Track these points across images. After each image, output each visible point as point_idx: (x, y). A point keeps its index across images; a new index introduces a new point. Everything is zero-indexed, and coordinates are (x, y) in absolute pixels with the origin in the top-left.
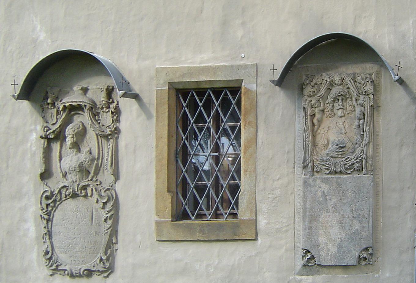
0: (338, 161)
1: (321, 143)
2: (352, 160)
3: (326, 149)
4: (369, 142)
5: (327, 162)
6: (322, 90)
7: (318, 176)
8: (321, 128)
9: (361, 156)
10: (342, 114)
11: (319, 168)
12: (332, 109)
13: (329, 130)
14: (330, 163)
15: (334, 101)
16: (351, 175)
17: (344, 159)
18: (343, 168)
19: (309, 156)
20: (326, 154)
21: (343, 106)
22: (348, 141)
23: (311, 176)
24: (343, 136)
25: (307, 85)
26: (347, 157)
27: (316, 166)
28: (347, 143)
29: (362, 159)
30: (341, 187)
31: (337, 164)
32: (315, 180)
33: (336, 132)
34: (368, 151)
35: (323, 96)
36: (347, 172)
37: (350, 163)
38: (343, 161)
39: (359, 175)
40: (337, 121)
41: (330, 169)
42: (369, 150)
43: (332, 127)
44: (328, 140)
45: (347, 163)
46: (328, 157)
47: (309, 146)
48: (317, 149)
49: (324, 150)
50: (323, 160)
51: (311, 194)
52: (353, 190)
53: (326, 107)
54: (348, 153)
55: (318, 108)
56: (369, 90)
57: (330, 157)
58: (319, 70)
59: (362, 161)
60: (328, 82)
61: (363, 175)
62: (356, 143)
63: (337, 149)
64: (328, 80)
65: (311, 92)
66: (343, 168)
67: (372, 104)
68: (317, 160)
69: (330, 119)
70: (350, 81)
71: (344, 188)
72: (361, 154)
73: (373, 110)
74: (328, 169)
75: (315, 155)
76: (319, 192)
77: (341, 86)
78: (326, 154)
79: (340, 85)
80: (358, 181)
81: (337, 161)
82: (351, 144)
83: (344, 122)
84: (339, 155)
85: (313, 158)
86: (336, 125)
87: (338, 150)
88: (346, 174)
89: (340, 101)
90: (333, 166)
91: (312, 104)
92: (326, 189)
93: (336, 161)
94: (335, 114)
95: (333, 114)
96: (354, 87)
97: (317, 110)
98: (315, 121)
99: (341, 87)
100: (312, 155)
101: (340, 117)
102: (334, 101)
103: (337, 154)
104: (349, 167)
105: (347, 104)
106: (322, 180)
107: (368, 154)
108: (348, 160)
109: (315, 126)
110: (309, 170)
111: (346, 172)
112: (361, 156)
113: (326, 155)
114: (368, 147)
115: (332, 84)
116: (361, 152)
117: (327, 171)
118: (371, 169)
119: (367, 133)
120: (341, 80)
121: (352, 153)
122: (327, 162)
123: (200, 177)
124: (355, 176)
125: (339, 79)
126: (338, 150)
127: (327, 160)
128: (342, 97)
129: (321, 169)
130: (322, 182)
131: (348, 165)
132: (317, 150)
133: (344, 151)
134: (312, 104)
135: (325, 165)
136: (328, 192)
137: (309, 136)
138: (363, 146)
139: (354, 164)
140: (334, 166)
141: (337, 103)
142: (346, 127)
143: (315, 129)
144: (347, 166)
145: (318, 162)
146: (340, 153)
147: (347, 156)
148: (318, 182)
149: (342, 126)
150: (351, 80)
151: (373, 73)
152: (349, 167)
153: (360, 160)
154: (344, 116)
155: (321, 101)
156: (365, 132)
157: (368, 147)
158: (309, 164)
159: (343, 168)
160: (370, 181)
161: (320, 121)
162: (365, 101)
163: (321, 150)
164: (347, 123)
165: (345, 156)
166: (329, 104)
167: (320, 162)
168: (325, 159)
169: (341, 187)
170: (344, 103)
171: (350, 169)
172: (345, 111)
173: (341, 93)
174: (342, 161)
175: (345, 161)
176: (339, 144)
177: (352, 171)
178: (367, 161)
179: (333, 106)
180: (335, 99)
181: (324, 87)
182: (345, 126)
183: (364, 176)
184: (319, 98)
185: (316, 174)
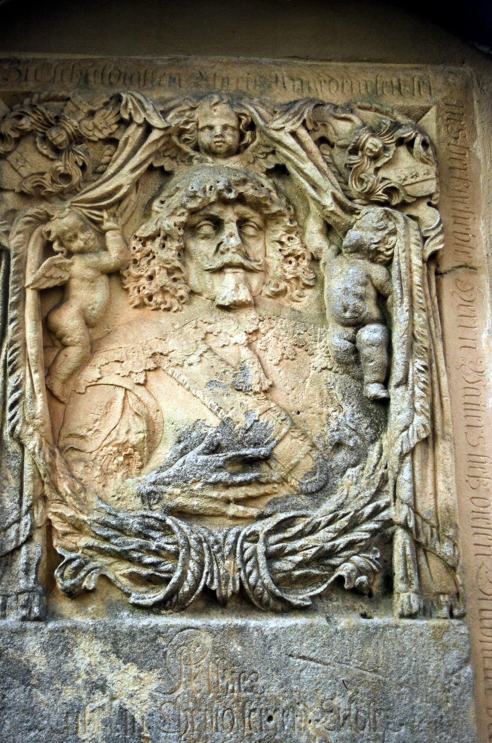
0: (225, 537)
1: (103, 435)
2: (322, 534)
3: (134, 470)
4: (429, 441)
5: (147, 537)
6: (122, 167)
7: (83, 620)
8: (100, 360)
9: (377, 511)
10: (243, 295)
11: (94, 576)
12: (178, 264)
13: (160, 373)
14: (176, 543)
15: (190, 229)
16: (319, 620)
17: (262, 527)
18: (259, 577)
19: (26, 504)
20: (141, 495)
21: (246, 256)
22: (284, 430)
23: (37, 619)
24: (250, 401)
25: (18, 141)
26: (282, 516)
27: (74, 564)
28: (278, 442)
29: (390, 530)
30: (251, 689)
31: (220, 550)
32: (62, 644)
33: (205, 379)
34: (424, 486)
35: (120, 201)
36: (285, 596)
37: (303, 548)
38: (262, 536)
39: (364, 616)
40: (209, 328)
41: (174, 580)
42: (430, 481)
43: (177, 356)
44: (149, 421)
45: (290, 546)
46: (157, 515)
47: (22, 446)
48: (79, 469)
49: (119, 475)
50: (121, 529)
51: (30, 730)
52: (335, 702)
53: (138, 256)
54: (283, 491)
55: (92, 259)
56: (410, 181)
57: (172, 511)
58: (91, 78)
59: (383, 538)
60: (155, 135)
61: (402, 616)
62: (338, 445)
63: (219, 468)
64: (156, 121)
65: (47, 176)
66: (264, 572)
67: (441, 246)
68: (78, 527)
69: (165, 319)
70: (294, 134)
71: (274, 690)
72: (382, 502)
73: (438, 282)
74: (152, 581)
75: (63, 501)
76: (88, 716)
77: (235, 158)
78: (141, 495)
79: (230, 153)
80: (369, 651)
81: (220, 536)
82: (306, 447)
83: (256, 331)
84: (228, 502)
85: (52, 517)
86: (203, 347)
87: (223, 476)
88: (277, 612)
89: (231, 228)
90: (191, 564)
91: (49, 233)
92: (145, 695)
93: (211, 533)
94: (192, 293)
95: (182, 292)
96: (319, 168)
97: (79, 266)
98: (68, 319)
99: (234, 162)
100: (44, 498)
101: (223, 308)
102: (190, 229)
103: (214, 494)
104: (297, 573)
105: (268, 249)
106: (114, 643)
107: (426, 504)
108: (294, 530)
109: (65, 346)
110: (22, 584)
111: (280, 599)
112: (377, 511)
113: (139, 500)
114: (424, 463)
115: (179, 146)
116: (379, 492)
117: (143, 589)
118: (452, 588)
119: (418, 392)
120: (233, 128)
121: (310, 494)
122: (147, 537)
123: (314, 576)
124: (343, 622)
125: (225, 122)
126: (223, 476)
127: (152, 528)
128: (241, 209)
129: (103, 577)
130: (117, 653)
131: (298, 558)
132: (78, 475)
133: (262, 484)
134: (53, 236)
135: (135, 555)
136: (156, 718)
137: (28, 394)
138: (394, 459)
139: (332, 553)
140: (201, 565)
141: (206, 237)
142: (271, 357)
143: (64, 368)
144: (290, 566)
145: (84, 541)
146: (241, 492)
147: (285, 509)
148: (87, 655)
149: (245, 353)
150: (302, 132)
151: (428, 109)
152: (297, 573)
153: (374, 532)
154: (253, 304)
155: (107, 225)
156: (404, 382)
157: (424, 463)
158: (18, 548)
159: (259, 577)
160: (455, 653)
161: (98, 328)
162: (393, 233)
163: (105, 474)
164: (273, 341)
165: (268, 511)
166: (158, 240)
167: (97, 536)
168: (134, 524)
169: (251, 689)
170: (251, 241)
171: (307, 580)
172: (255, 280)
173: (241, 189)
174: (253, 537)
175: (273, 539)
176: (224, 443)
177: (319, 591)
178: (422, 540)
179: (183, 252)
180: (196, 219)
181: (134, 152)
182: (262, 354)
183: (404, 628)
184: (100, 209)
185: (66, 606)
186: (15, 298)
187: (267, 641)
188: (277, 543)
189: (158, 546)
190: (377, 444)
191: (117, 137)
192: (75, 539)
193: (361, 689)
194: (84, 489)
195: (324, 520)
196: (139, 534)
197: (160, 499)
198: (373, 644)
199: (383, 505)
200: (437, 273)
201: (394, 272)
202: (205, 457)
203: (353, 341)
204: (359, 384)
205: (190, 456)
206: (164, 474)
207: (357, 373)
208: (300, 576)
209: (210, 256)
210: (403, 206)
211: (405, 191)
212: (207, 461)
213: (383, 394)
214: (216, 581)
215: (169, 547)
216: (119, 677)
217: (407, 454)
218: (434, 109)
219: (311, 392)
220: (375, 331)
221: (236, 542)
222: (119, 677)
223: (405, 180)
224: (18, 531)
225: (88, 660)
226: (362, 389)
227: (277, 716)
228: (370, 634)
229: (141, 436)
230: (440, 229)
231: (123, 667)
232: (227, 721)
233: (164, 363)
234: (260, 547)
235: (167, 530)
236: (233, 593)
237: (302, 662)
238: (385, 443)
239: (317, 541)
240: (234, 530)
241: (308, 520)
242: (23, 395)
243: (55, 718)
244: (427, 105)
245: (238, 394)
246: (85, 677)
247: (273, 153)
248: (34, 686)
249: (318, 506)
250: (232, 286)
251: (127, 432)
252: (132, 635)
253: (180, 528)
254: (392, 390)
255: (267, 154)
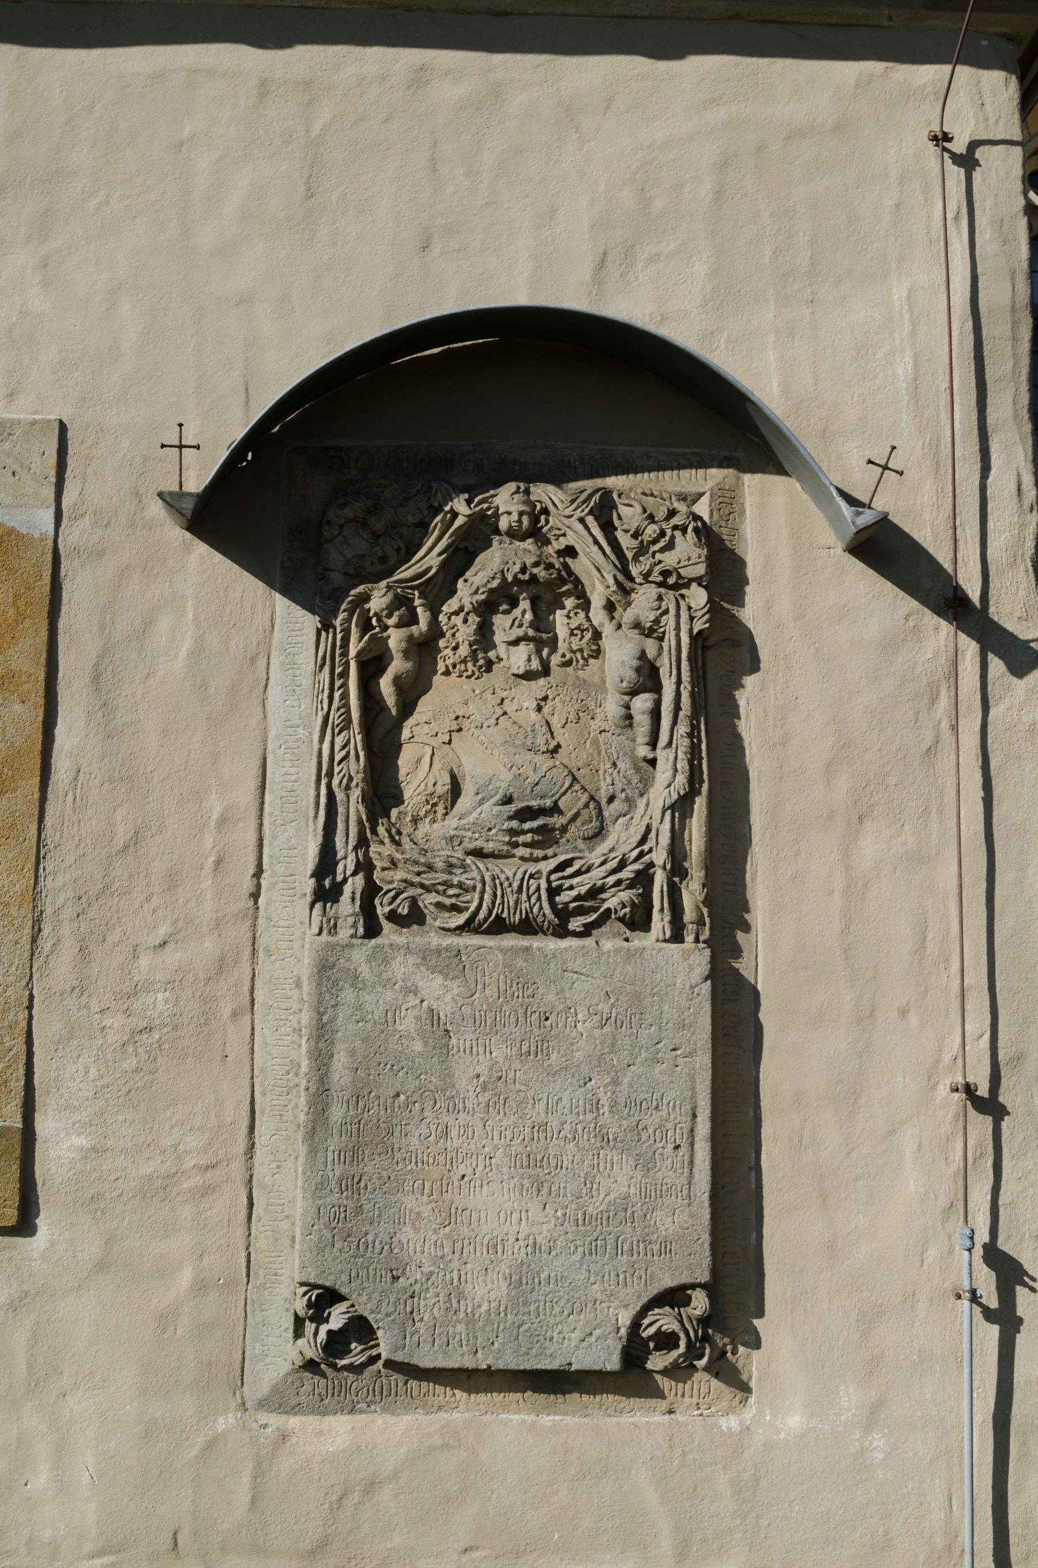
5: (450, 873)
16: (589, 942)
22: (567, 785)
26: (562, 858)
37: (579, 885)
40: (504, 694)
44: (454, 778)
45: (567, 883)
46: (459, 855)
49: (428, 820)
71: (551, 997)
75: (382, 843)
80: (629, 968)
81: (511, 875)
92: (448, 998)
93: (502, 871)
115: (479, 534)
139: (602, 889)
144: (567, 899)
148: (401, 967)
153: (638, 873)
159: (541, 908)
166: (462, 615)
171: (581, 911)
175: (553, 877)
184: (412, 588)
186: (341, 668)
187: (547, 959)
188: (558, 879)
189: (460, 882)
190: (645, 796)
191: (427, 520)
192: (391, 873)
193: (621, 997)
194: (399, 833)
195: (598, 862)
196: (443, 871)
197: (461, 842)
198: (633, 962)
199: (646, 850)
200: (704, 647)
201: (665, 645)
202: (501, 807)
203: (628, 707)
204: (632, 745)
205: (486, 806)
206: (464, 821)
207: (631, 736)
208: (575, 908)
209: (507, 629)
210: (676, 587)
211: (679, 574)
212: (500, 811)
213: (651, 756)
214: (506, 911)
215: (468, 882)
216: (428, 984)
217: (668, 808)
218: (708, 495)
219: (590, 751)
220: (646, 701)
221: (523, 879)
222: (428, 984)
223: (679, 563)
224: (345, 866)
225: (403, 970)
226: (635, 749)
227: (553, 1018)
228: (630, 955)
229: (447, 787)
230: (706, 609)
231: (431, 976)
232: (513, 1019)
233: (465, 724)
234: (544, 885)
235: (465, 868)
236: (521, 919)
237: (575, 976)
238: (652, 796)
239: (590, 879)
240: (522, 870)
241: (583, 861)
242: (348, 753)
243: (377, 1014)
244: (702, 491)
245: (529, 753)
246: (400, 983)
247: (564, 535)
248: (360, 989)
249: (591, 850)
250: (525, 657)
251: (434, 785)
252: (438, 952)
253: (478, 867)
254: (658, 751)
255: (560, 536)
